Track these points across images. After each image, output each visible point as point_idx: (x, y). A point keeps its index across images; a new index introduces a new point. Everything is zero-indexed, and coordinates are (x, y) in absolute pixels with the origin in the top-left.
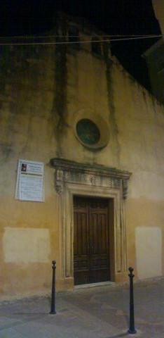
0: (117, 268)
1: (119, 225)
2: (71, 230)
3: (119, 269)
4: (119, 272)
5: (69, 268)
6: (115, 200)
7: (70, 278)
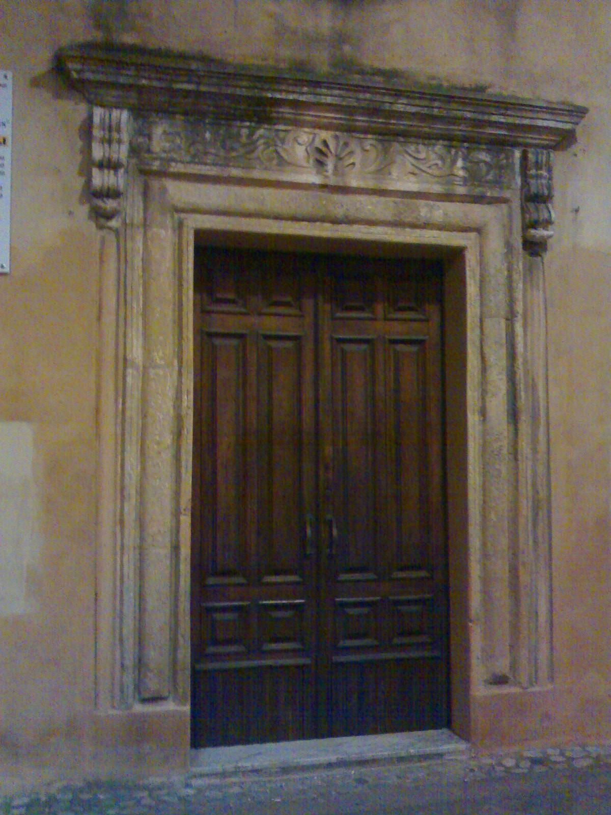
0: (489, 656)
1: (498, 406)
2: (178, 435)
3: (502, 666)
4: (500, 680)
5: (156, 656)
6: (471, 259)
7: (170, 706)
